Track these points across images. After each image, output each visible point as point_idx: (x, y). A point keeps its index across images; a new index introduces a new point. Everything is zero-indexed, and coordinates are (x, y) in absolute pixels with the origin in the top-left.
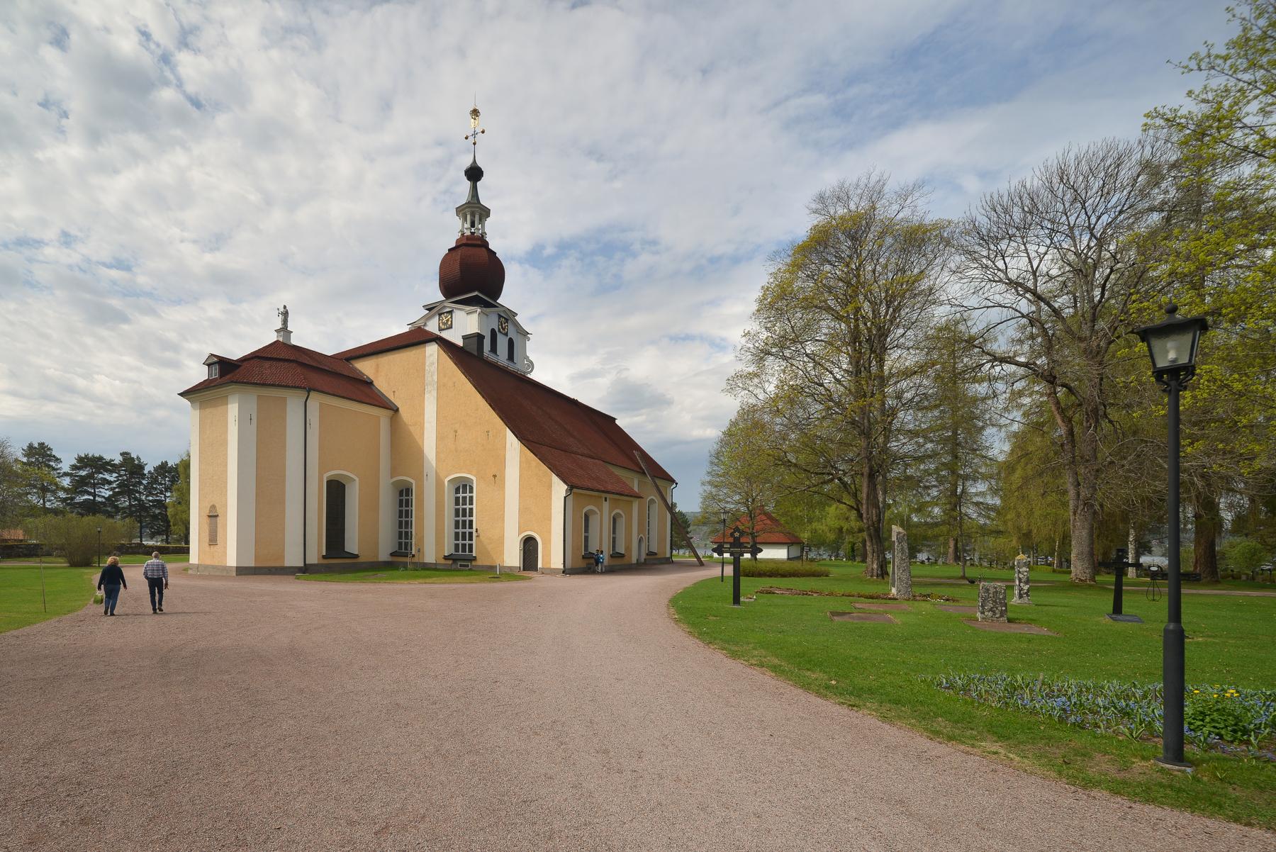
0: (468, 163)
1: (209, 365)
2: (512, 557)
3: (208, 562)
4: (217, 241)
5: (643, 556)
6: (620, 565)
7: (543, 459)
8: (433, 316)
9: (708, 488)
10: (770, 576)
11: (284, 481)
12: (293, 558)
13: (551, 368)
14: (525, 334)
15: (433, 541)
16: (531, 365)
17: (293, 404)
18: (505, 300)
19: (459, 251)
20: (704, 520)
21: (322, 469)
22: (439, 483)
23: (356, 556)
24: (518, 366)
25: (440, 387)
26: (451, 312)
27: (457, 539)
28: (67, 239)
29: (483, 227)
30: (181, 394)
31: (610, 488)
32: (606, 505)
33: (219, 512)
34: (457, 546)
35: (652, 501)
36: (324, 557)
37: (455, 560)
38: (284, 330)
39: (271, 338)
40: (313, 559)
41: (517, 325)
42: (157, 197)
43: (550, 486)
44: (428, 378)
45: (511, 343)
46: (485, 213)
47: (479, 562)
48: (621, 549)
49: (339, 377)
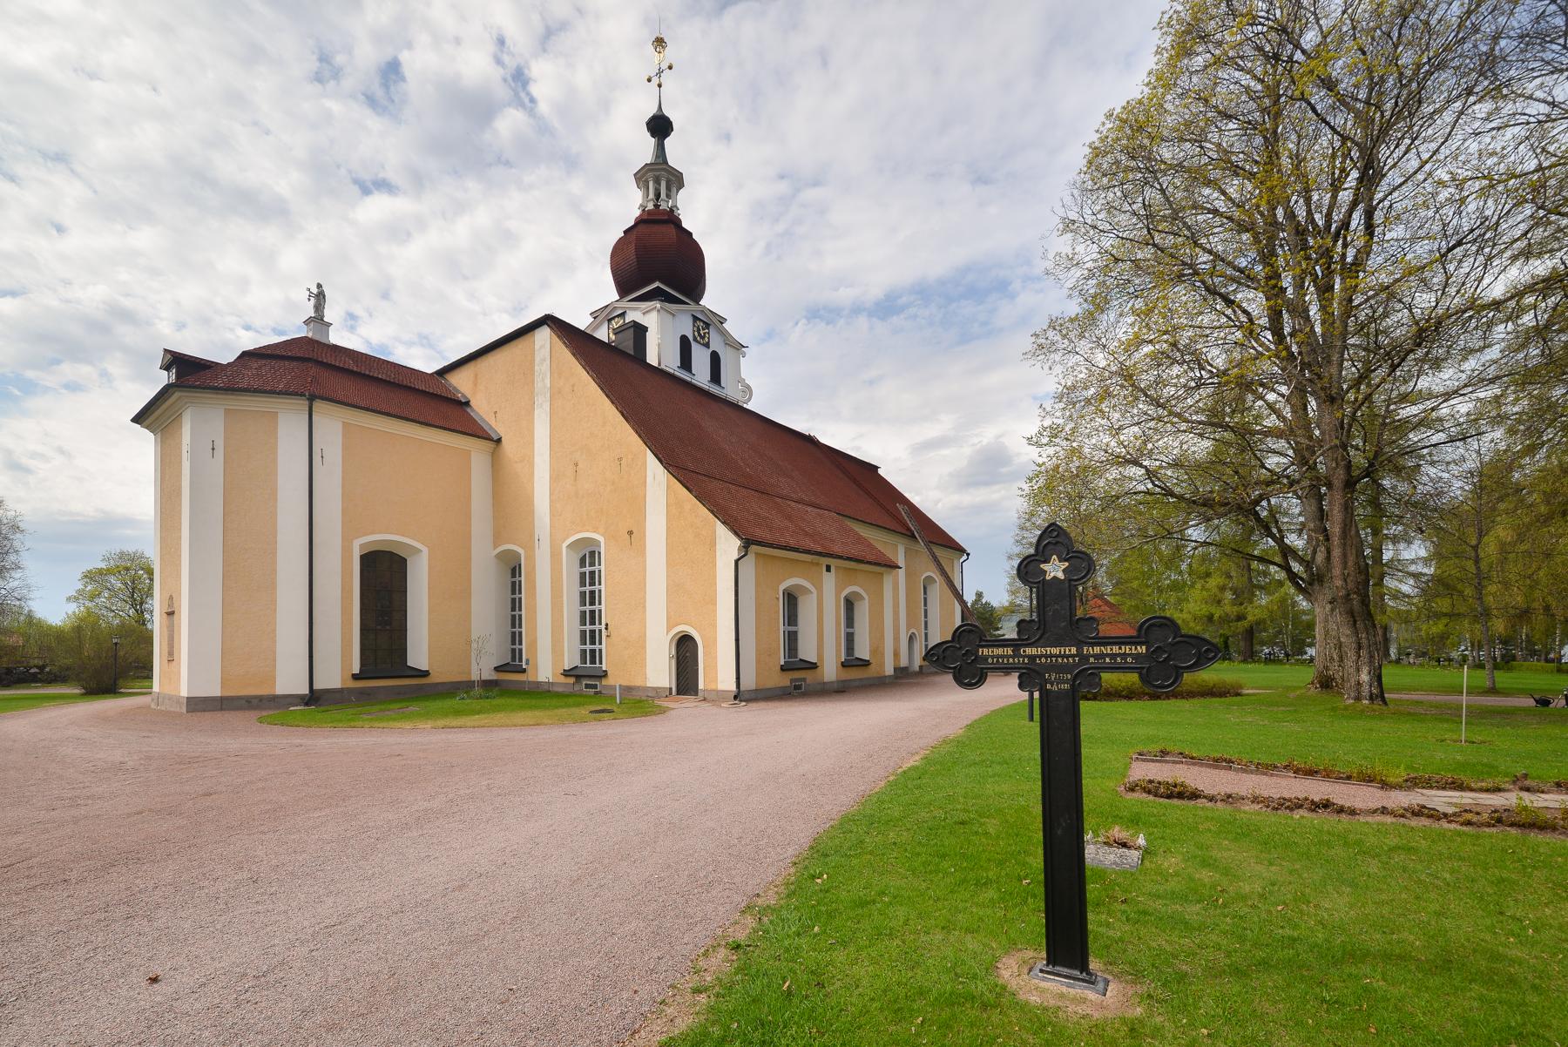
0: (652, 111)
2: (659, 672)
6: (860, 679)
7: (702, 497)
8: (601, 324)
11: (274, 553)
12: (290, 681)
13: (768, 386)
14: (738, 347)
15: (550, 654)
16: (748, 389)
17: (289, 423)
18: (711, 300)
22: (555, 555)
23: (426, 674)
24: (729, 390)
25: (555, 394)
31: (837, 549)
32: (829, 581)
35: (929, 580)
36: (355, 677)
37: (578, 677)
38: (318, 319)
39: (294, 327)
40: (332, 676)
41: (725, 335)
43: (713, 544)
44: (538, 385)
45: (715, 359)
48: (862, 651)
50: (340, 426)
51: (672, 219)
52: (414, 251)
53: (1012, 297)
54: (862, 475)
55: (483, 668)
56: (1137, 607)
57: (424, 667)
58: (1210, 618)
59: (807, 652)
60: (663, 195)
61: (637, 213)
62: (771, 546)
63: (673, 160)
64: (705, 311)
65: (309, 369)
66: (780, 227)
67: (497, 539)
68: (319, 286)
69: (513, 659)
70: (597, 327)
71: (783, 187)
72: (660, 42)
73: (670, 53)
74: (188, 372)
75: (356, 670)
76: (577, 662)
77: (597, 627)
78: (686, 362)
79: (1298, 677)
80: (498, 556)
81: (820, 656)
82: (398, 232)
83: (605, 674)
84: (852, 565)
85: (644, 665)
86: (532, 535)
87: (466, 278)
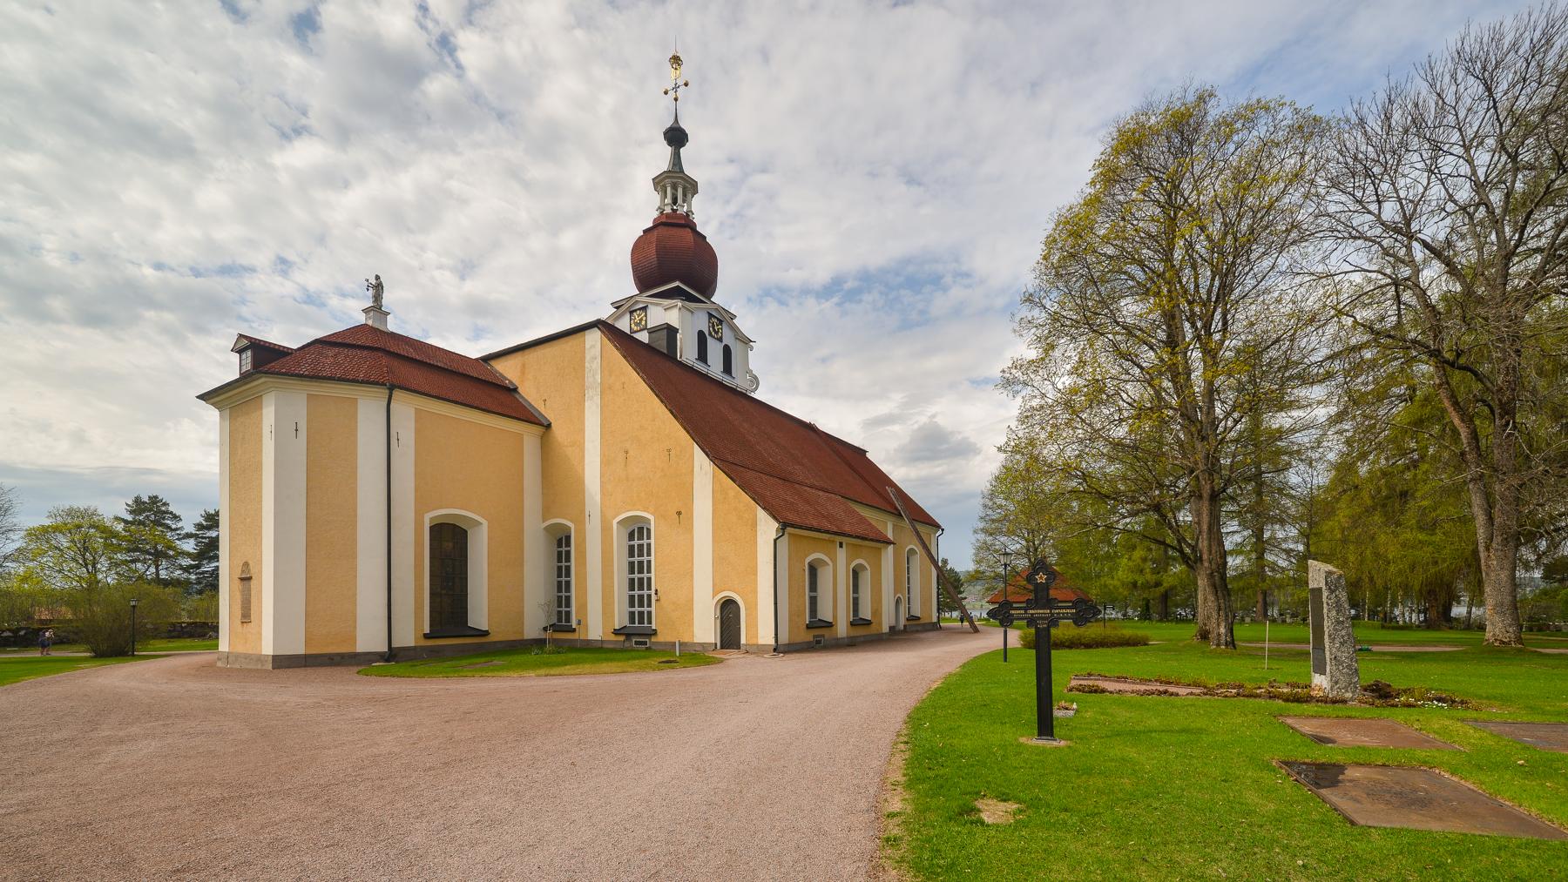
1: (240, 352)
2: (705, 630)
3: (240, 649)
4: (466, 269)
5: (902, 622)
6: (865, 636)
7: (744, 486)
9: (982, 536)
10: (1070, 647)
12: (370, 639)
13: (785, 384)
14: (746, 342)
15: (599, 613)
17: (368, 408)
18: (721, 297)
19: (655, 232)
20: (976, 577)
21: (421, 507)
22: (606, 528)
23: (486, 633)
24: (739, 381)
26: (644, 309)
27: (632, 604)
28: (283, 265)
29: (690, 206)
30: (201, 397)
31: (847, 529)
32: (842, 554)
33: (253, 572)
34: (632, 614)
35: (912, 552)
36: (426, 636)
37: (629, 636)
38: (377, 308)
39: (352, 313)
40: (407, 637)
41: (735, 329)
42: (396, 218)
43: (754, 525)
44: (589, 380)
45: (727, 351)
46: (691, 187)
47: (660, 638)
48: (865, 613)
49: (479, 386)
50: (412, 411)
51: (687, 223)
52: (353, 199)
53: (945, 290)
54: (852, 458)
55: (533, 624)
56: (1077, 576)
57: (485, 628)
58: (1135, 585)
59: (825, 613)
60: (680, 201)
61: (656, 214)
62: (800, 527)
63: (689, 170)
64: (719, 309)
65: (374, 359)
66: (732, 208)
67: (546, 512)
68: (377, 278)
69: (560, 620)
70: (619, 317)
71: (731, 171)
72: (676, 60)
73: (686, 72)
74: (264, 358)
75: (427, 630)
76: (626, 623)
77: (645, 592)
78: (703, 356)
79: (1189, 632)
80: (546, 529)
81: (835, 617)
82: (335, 179)
83: (655, 633)
84: (859, 541)
85: (691, 624)
86: (583, 511)
87: (410, 231)
